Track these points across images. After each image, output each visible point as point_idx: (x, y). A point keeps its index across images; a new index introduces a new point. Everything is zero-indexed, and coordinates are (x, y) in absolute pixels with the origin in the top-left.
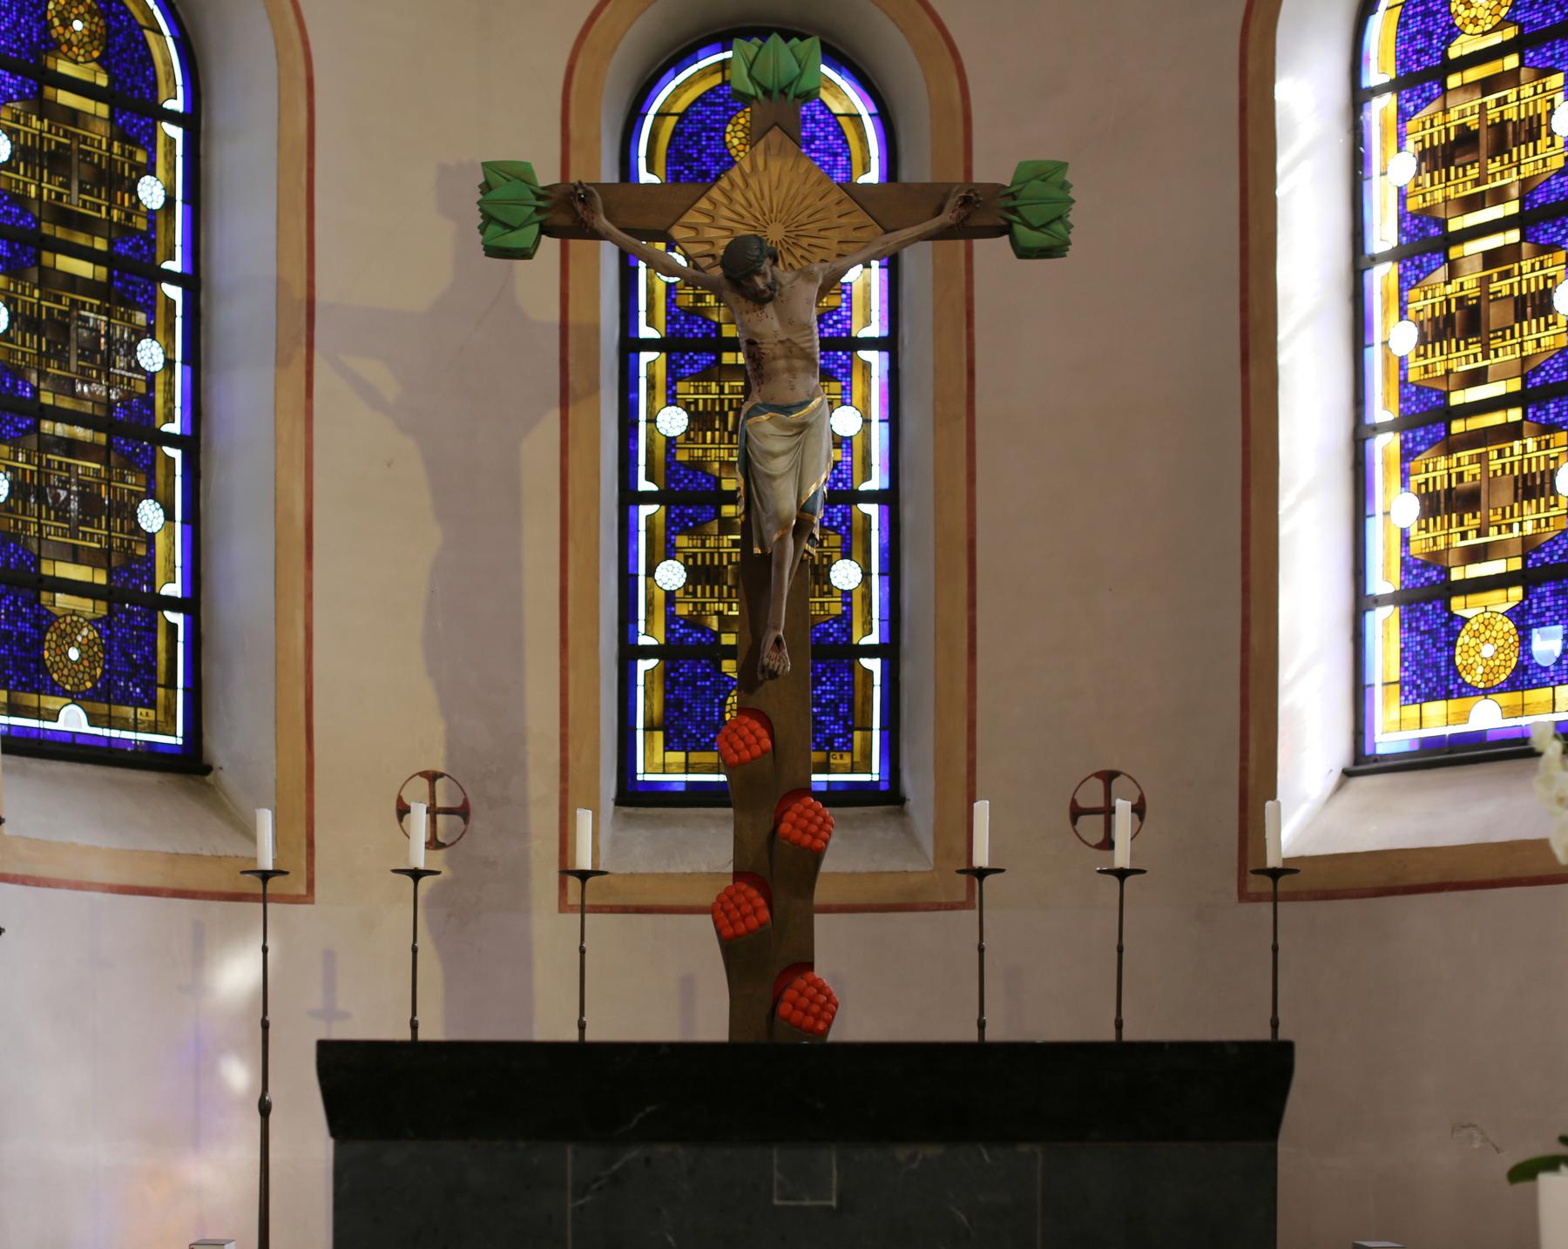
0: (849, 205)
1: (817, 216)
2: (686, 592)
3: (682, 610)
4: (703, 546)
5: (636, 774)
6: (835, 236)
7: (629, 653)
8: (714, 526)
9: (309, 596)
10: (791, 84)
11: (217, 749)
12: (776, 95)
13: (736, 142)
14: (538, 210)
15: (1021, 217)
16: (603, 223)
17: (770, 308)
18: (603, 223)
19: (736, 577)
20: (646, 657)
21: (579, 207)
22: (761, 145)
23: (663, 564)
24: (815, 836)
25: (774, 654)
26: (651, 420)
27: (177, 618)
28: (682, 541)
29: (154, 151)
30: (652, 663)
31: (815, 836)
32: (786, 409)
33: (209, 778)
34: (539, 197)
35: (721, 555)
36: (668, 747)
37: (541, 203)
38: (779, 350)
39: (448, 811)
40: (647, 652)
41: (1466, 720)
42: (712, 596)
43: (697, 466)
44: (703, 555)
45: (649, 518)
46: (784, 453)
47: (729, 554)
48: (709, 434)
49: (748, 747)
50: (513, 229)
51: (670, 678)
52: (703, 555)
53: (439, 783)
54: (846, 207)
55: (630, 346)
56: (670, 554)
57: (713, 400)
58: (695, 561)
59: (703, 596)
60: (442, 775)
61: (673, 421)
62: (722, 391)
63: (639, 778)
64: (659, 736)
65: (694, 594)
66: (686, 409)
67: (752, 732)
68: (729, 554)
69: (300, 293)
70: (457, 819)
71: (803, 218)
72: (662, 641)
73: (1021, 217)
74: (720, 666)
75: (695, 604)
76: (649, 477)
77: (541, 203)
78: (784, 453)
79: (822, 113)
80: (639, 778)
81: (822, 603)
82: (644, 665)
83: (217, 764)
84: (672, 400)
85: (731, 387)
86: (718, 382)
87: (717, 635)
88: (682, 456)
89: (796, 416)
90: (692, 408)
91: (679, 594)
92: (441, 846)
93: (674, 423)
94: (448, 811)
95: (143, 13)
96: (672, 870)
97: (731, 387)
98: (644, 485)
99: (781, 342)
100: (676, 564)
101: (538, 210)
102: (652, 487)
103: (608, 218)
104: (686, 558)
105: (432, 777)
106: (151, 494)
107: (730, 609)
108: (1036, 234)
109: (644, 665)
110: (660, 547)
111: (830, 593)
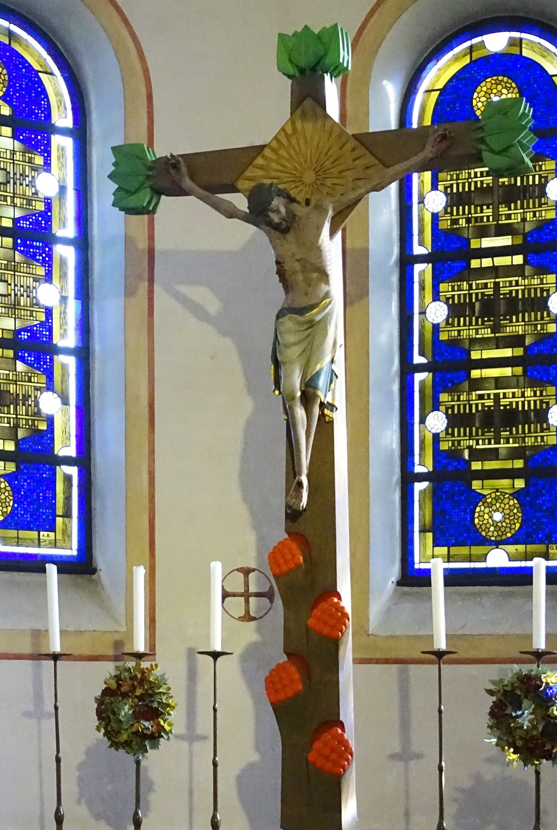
0: (361, 151)
2: (447, 433)
3: (444, 446)
4: (459, 400)
5: (413, 564)
6: (350, 175)
7: (408, 478)
9: (152, 452)
10: (318, 63)
11: (100, 559)
12: (308, 72)
13: (480, 105)
14: (148, 177)
16: (187, 183)
17: (290, 236)
18: (187, 183)
22: (298, 112)
23: (431, 415)
24: (333, 627)
26: (423, 313)
27: (73, 471)
28: (444, 397)
29: (49, 155)
31: (333, 627)
32: (301, 311)
33: (94, 577)
34: (150, 168)
35: (471, 406)
36: (436, 544)
37: (150, 173)
38: (297, 266)
39: (258, 595)
40: (421, 477)
41: (485, 561)
42: (465, 435)
43: (454, 343)
44: (459, 406)
45: (422, 383)
46: (295, 344)
47: (477, 405)
48: (462, 319)
49: (286, 561)
51: (437, 496)
52: (459, 406)
53: (251, 575)
54: (357, 153)
55: (406, 261)
56: (436, 408)
57: (465, 295)
58: (453, 411)
59: (459, 435)
60: (254, 570)
63: (417, 566)
64: (430, 536)
67: (290, 550)
69: (143, 245)
70: (265, 601)
72: (431, 469)
73: (487, 145)
74: (471, 485)
76: (422, 353)
77: (150, 173)
78: (295, 344)
80: (417, 566)
81: (542, 437)
82: (419, 487)
83: (99, 568)
84: (436, 297)
85: (477, 285)
86: (468, 281)
87: (468, 463)
88: (443, 337)
89: (308, 315)
91: (442, 435)
92: (254, 619)
93: (438, 314)
94: (258, 595)
95: (38, 62)
96: (421, 633)
97: (477, 285)
98: (418, 359)
99: (298, 260)
100: (440, 414)
104: (447, 409)
105: (246, 572)
106: (50, 387)
107: (478, 444)
109: (419, 487)
111: (548, 429)
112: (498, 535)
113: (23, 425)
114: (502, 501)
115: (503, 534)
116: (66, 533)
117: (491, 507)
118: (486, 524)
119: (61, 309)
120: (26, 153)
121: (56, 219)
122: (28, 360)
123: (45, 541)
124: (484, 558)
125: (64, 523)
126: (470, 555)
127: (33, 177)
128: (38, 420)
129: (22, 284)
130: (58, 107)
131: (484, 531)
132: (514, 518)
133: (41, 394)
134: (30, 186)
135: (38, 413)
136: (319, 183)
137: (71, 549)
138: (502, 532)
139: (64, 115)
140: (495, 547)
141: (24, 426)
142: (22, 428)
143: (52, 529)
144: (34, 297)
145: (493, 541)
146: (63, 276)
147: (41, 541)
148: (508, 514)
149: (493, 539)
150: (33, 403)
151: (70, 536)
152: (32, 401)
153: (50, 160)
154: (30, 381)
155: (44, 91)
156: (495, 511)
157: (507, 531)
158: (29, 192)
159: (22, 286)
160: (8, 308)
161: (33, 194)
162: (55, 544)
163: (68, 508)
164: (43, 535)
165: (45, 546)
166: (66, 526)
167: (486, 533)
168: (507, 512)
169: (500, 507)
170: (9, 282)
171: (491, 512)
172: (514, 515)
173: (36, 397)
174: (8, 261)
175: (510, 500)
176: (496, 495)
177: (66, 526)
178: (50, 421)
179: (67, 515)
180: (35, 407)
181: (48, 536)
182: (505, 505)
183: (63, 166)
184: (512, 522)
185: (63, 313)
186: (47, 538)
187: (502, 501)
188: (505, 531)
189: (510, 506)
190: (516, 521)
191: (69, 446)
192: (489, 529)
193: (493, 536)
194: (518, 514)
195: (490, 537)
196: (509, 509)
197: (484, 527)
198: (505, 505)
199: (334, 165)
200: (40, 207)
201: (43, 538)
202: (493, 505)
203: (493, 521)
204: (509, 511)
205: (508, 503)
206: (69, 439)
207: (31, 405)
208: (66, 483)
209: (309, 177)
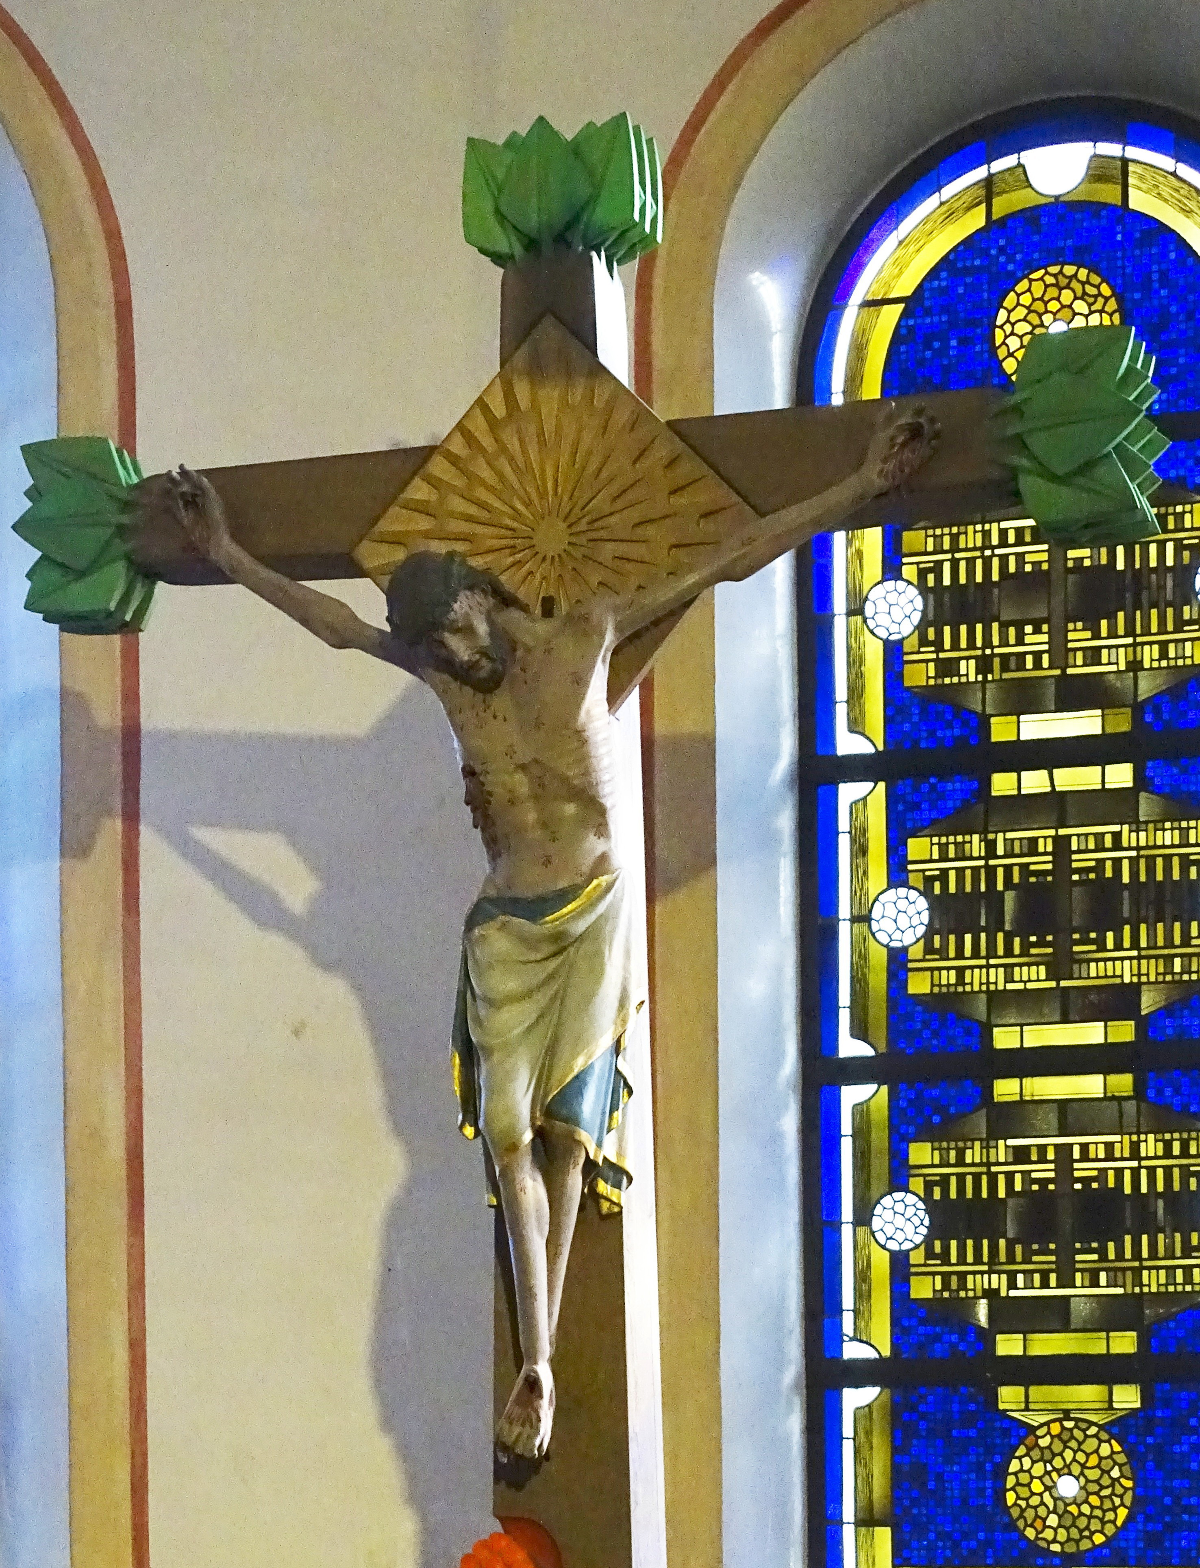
1: (630, 496)
2: (930, 1254)
7: (825, 1373)
8: (980, 1121)
12: (547, 249)
15: (1033, 458)
16: (226, 548)
17: (501, 701)
19: (1020, 1220)
20: (857, 1384)
21: (186, 517)
23: (887, 1201)
25: (517, 1411)
28: (921, 1153)
30: (867, 1395)
34: (126, 506)
35: (993, 1179)
37: (125, 519)
42: (978, 1260)
45: (861, 1111)
50: (81, 574)
51: (906, 1425)
56: (899, 1180)
57: (975, 870)
59: (962, 1261)
61: (902, 917)
62: (991, 850)
65: (944, 1257)
66: (926, 892)
68: (1010, 1176)
71: (601, 503)
72: (886, 1352)
73: (1033, 458)
75: (946, 1276)
79: (938, 278)
82: (855, 1399)
86: (984, 832)
88: (918, 985)
90: (937, 888)
101: (121, 531)
102: (863, 1050)
103: (236, 537)
104: (929, 1186)
108: (1065, 492)
110: (880, 1165)
112: (1069, 1539)
114: (1080, 1444)
118: (1035, 1508)
132: (1113, 1493)
136: (578, 553)
138: (1081, 1531)
148: (1097, 1482)
182: (1088, 1455)
184: (1107, 1505)
187: (1080, 1444)
188: (1087, 1528)
189: (1101, 1458)
190: (1117, 1501)
192: (1044, 1520)
193: (1054, 1541)
194: (1123, 1481)
196: (1098, 1466)
197: (1030, 1514)
198: (1088, 1455)
199: (619, 504)
203: (1056, 1500)
205: (1096, 1451)
209: (553, 538)
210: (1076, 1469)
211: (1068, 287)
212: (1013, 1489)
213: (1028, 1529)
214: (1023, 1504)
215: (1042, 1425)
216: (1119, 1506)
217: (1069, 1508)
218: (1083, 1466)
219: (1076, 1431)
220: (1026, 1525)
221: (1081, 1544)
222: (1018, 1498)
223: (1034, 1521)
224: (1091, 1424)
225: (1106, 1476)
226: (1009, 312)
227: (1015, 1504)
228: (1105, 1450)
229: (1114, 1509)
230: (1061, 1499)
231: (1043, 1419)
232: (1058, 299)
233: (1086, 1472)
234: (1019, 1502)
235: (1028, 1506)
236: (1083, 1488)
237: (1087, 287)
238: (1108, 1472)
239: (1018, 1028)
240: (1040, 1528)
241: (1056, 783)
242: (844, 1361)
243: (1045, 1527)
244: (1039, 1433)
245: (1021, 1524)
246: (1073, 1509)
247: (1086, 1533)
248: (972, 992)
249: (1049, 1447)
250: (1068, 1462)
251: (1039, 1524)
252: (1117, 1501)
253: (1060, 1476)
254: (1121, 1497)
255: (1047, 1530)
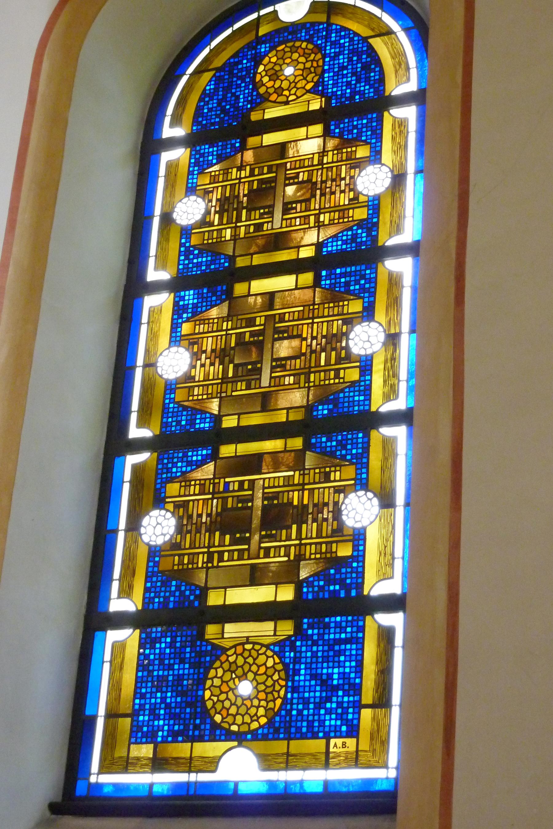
56: (159, 502)
106: (362, 484)
112: (243, 723)
113: (311, 554)
114: (255, 659)
115: (252, 721)
116: (380, 739)
117: (234, 672)
118: (223, 702)
119: (386, 356)
120: (342, 149)
121: (385, 224)
122: (326, 447)
123: (338, 755)
124: (211, 764)
125: (374, 718)
126: (191, 758)
127: (352, 178)
128: (337, 542)
129: (315, 334)
130: (396, 71)
131: (219, 713)
132: (274, 690)
133: (345, 497)
134: (347, 190)
135: (339, 530)
137: (386, 767)
138: (251, 717)
139: (404, 79)
140: (235, 743)
141: (313, 556)
142: (310, 559)
143: (353, 731)
144: (342, 348)
145: (234, 732)
146: (394, 302)
147: (331, 755)
148: (264, 683)
149: (234, 728)
150: (331, 515)
151: (385, 743)
152: (328, 512)
153: (381, 146)
154: (327, 479)
155: (376, 60)
156: (240, 678)
157: (259, 714)
158: (344, 200)
159: (316, 338)
160: (299, 374)
161: (350, 200)
162: (355, 760)
163: (384, 689)
164: (335, 745)
165: (338, 766)
166: (378, 725)
167: (223, 718)
168: (261, 679)
169: (250, 670)
170: (304, 335)
171: (234, 679)
172: (273, 685)
173: (336, 504)
174: (304, 306)
175: (268, 657)
176: (244, 649)
177: (378, 725)
178: (358, 538)
179: (382, 702)
180: (196, 533)
181: (344, 745)
182: (259, 667)
183: (400, 147)
184: (270, 697)
185: (392, 362)
186: (342, 750)
187: (255, 659)
188: (256, 714)
189: (267, 668)
190: (276, 694)
191: (392, 577)
192: (228, 710)
193: (234, 723)
194: (280, 681)
195: (230, 725)
196: (265, 673)
197: (219, 706)
198: (259, 667)
200: (361, 214)
201: (335, 750)
202: (238, 667)
203: (236, 696)
204: (265, 677)
205: (265, 664)
206: (392, 565)
207: (326, 520)
208: (382, 645)
210: (251, 676)
211: (296, 52)
212: (209, 689)
213: (217, 715)
214: (215, 699)
215: (231, 648)
216: (277, 698)
217: (245, 702)
218: (256, 674)
219: (253, 651)
220: (216, 713)
221: (251, 725)
222: (212, 695)
223: (221, 710)
224: (262, 645)
225: (270, 679)
226: (265, 66)
227: (210, 699)
228: (270, 663)
229: (274, 700)
230: (241, 696)
231: (231, 644)
232: (290, 58)
233: (257, 677)
234: (212, 697)
235: (218, 700)
236: (256, 688)
237: (306, 51)
238: (271, 677)
239: (236, 417)
240: (225, 716)
241: (301, 142)
242: (110, 613)
243: (228, 715)
244: (229, 653)
245: (212, 712)
246: (248, 703)
247: (255, 718)
248: (225, 241)
249: (235, 662)
250: (246, 671)
251: (224, 712)
252: (276, 694)
253: (240, 681)
254: (278, 692)
255: (229, 717)
